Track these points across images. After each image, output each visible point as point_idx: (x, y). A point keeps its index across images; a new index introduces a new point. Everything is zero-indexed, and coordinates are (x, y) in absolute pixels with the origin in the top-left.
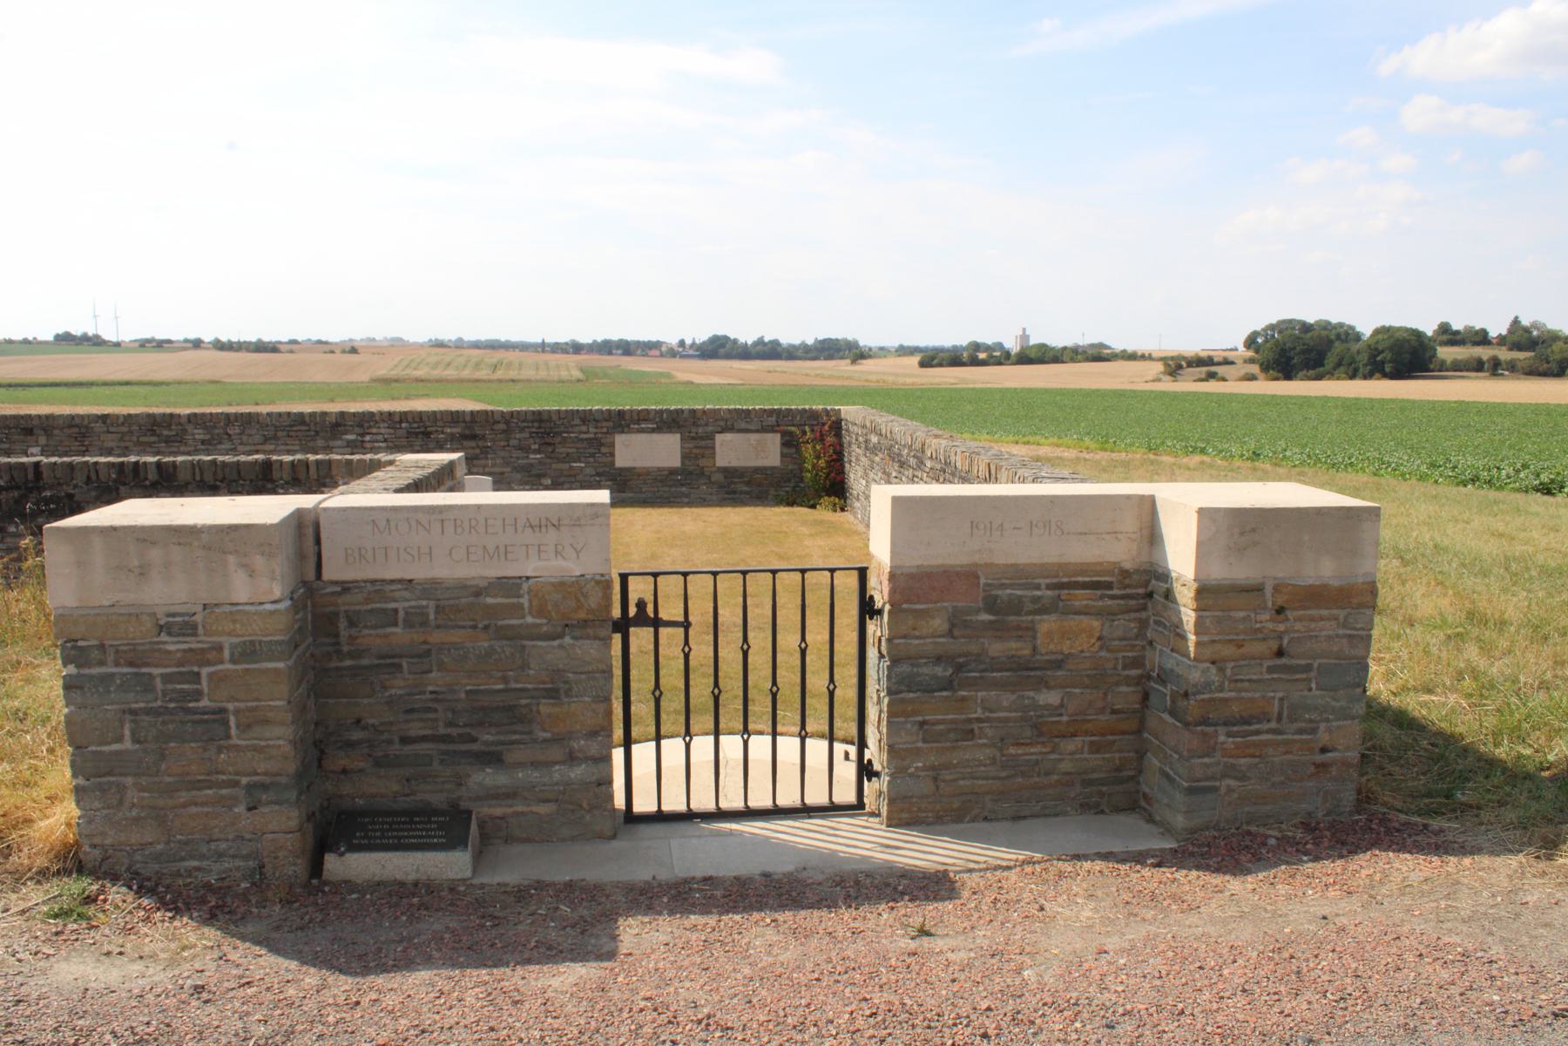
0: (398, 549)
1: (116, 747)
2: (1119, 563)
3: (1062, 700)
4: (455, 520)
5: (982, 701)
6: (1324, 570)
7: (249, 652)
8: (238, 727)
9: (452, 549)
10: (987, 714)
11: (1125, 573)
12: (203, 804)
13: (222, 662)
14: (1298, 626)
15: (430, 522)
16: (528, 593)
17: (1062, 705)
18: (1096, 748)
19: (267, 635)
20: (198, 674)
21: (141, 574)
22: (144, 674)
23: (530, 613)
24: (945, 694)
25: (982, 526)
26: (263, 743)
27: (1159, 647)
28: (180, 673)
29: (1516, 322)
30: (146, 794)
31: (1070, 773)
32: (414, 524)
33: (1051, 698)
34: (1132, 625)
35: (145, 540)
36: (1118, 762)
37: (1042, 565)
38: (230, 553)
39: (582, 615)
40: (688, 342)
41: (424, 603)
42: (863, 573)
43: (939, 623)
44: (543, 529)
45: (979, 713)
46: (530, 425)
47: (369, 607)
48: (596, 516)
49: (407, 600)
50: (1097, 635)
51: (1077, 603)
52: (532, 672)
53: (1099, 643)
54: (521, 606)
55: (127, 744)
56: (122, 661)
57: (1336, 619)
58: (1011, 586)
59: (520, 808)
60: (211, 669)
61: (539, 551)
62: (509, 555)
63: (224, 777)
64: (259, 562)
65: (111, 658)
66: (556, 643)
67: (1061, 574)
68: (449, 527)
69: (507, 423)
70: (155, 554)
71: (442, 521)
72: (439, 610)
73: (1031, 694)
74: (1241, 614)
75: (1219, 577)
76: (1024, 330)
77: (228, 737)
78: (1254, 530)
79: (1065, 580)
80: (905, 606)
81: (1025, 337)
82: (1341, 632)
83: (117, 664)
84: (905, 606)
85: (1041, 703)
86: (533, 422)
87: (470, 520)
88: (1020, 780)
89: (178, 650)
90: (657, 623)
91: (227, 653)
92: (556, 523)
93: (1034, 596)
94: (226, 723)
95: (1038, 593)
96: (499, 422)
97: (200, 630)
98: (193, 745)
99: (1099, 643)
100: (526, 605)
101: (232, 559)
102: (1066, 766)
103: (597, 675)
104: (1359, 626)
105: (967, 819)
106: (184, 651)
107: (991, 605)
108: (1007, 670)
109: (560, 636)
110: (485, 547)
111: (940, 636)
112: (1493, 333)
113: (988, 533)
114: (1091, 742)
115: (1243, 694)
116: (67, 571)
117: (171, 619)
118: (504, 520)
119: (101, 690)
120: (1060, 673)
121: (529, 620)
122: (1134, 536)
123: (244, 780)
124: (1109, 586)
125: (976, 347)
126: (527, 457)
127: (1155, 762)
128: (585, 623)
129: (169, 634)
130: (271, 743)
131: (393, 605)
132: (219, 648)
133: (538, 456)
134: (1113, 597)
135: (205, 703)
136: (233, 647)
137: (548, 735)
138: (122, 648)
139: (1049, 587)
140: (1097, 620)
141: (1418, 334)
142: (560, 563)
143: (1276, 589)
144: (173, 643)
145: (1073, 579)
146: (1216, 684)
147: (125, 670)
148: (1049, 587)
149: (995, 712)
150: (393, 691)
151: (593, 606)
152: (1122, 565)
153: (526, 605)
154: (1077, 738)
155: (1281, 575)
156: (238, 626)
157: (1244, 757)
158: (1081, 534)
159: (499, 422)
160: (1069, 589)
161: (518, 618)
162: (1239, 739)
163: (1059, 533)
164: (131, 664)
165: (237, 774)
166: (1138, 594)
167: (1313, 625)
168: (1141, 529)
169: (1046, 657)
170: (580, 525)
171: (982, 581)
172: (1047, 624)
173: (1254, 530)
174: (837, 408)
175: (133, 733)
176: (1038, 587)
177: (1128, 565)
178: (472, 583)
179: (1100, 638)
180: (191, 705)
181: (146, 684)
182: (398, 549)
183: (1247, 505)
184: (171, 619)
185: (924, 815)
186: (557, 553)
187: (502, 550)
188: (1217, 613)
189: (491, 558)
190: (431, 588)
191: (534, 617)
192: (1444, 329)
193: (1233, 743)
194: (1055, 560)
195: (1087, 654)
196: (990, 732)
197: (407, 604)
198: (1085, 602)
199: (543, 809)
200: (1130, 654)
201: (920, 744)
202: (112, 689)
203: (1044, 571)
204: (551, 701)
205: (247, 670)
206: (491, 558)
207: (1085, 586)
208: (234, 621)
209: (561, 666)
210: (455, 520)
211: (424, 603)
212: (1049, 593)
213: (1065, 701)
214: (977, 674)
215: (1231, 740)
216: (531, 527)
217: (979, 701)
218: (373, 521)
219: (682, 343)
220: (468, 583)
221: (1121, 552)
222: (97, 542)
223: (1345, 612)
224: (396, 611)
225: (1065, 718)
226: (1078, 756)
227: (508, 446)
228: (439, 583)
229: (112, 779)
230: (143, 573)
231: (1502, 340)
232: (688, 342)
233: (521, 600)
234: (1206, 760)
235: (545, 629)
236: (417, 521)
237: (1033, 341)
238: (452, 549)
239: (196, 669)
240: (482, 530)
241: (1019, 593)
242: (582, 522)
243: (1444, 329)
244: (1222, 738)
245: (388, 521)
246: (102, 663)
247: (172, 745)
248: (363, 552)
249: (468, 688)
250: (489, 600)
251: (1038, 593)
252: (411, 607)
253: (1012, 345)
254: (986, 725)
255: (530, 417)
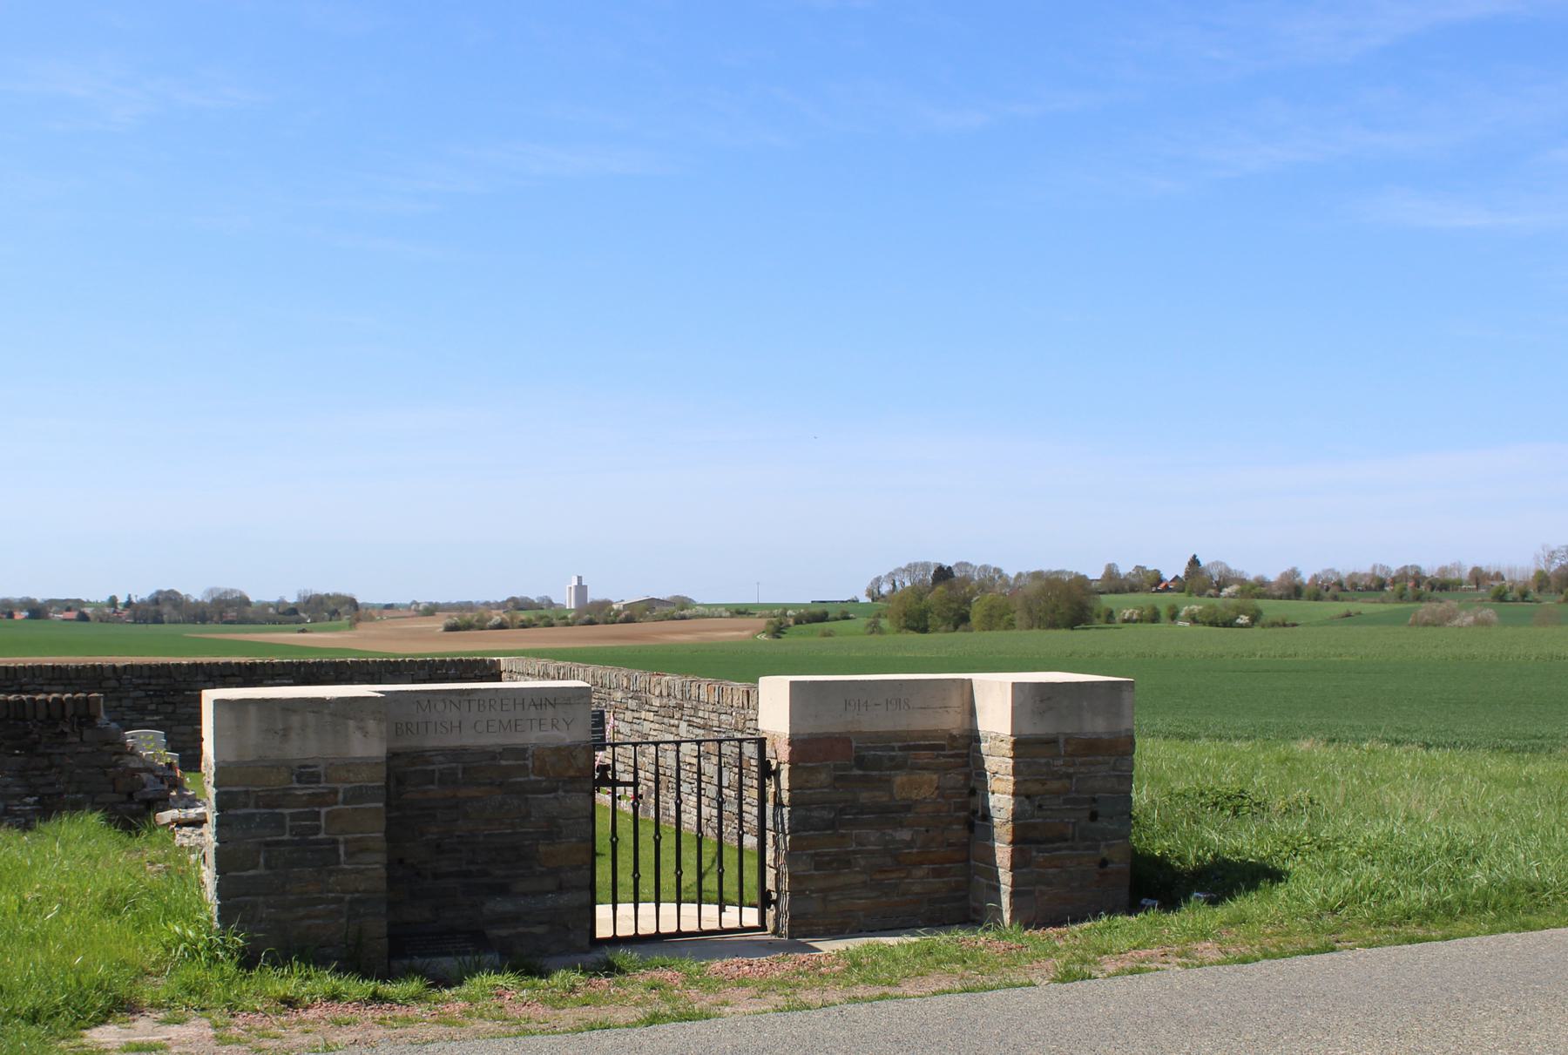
0: (436, 723)
1: (251, 872)
2: (949, 730)
3: (912, 835)
4: (479, 700)
5: (856, 837)
6: (1096, 725)
7: (357, 795)
8: (346, 854)
9: (476, 723)
10: (859, 848)
11: (953, 738)
12: (316, 917)
13: (336, 804)
14: (1083, 769)
15: (460, 702)
16: (532, 756)
17: (913, 840)
18: (937, 873)
19: (373, 782)
20: (319, 813)
21: (285, 735)
22: (277, 814)
23: (533, 772)
24: (829, 832)
25: (853, 703)
26: (363, 867)
27: (981, 792)
28: (301, 813)
29: (1194, 562)
30: (273, 910)
31: (921, 894)
32: (448, 703)
33: (905, 835)
34: (960, 777)
35: (288, 710)
36: (953, 884)
37: (895, 732)
38: (351, 719)
39: (572, 773)
40: (122, 599)
41: (454, 765)
42: (761, 743)
43: (823, 777)
44: (544, 707)
45: (854, 847)
46: (147, 681)
47: (413, 769)
48: (582, 697)
49: (442, 763)
50: (936, 785)
51: (920, 761)
52: (533, 819)
53: (937, 792)
54: (526, 766)
55: (261, 871)
56: (261, 804)
57: (1108, 763)
58: (874, 749)
59: (521, 930)
60: (329, 809)
61: (540, 725)
62: (518, 727)
63: (333, 895)
64: (371, 725)
65: (252, 802)
66: (552, 795)
67: (908, 739)
68: (474, 706)
69: (119, 680)
70: (295, 720)
71: (469, 701)
72: (465, 770)
73: (890, 831)
74: (1043, 761)
75: (1027, 733)
76: (580, 578)
77: (338, 863)
78: (1049, 699)
79: (912, 743)
80: (800, 764)
81: (581, 590)
82: (1112, 773)
83: (257, 807)
84: (800, 764)
85: (897, 838)
86: (150, 677)
87: (490, 700)
88: (884, 899)
89: (304, 795)
90: (615, 783)
91: (340, 797)
92: (552, 702)
93: (890, 756)
94: (336, 851)
95: (894, 753)
96: (109, 679)
97: (323, 779)
98: (311, 869)
99: (937, 792)
100: (531, 766)
101: (351, 723)
102: (917, 888)
103: (581, 820)
104: (1124, 768)
105: (847, 931)
106: (309, 795)
107: (860, 762)
108: (873, 813)
109: (555, 790)
110: (500, 722)
111: (825, 787)
112: (1168, 576)
113: (857, 708)
114: (933, 869)
115: (1048, 820)
116: (229, 733)
117: (302, 770)
118: (515, 700)
119: (244, 826)
120: (909, 815)
121: (532, 777)
122: (958, 710)
123: (348, 897)
124: (942, 747)
125: (518, 604)
126: (143, 719)
127: (982, 880)
128: (573, 780)
129: (299, 781)
130: (370, 867)
131: (431, 767)
132: (335, 792)
133: (156, 718)
134: (945, 756)
135: (322, 836)
136: (346, 791)
137: (543, 869)
138: (260, 794)
139: (901, 749)
140: (935, 774)
141: (1082, 581)
142: (556, 732)
143: (1067, 741)
144: (302, 789)
145: (918, 743)
146: (1030, 812)
147: (263, 811)
148: (901, 749)
149: (865, 846)
150: (429, 836)
151: (581, 766)
152: (952, 731)
153: (531, 766)
154: (924, 866)
155: (1069, 731)
156: (351, 775)
157: (1051, 868)
158: (922, 708)
159: (109, 679)
160: (914, 750)
161: (524, 777)
162: (1046, 854)
163: (906, 707)
164: (266, 806)
165: (343, 892)
166: (963, 754)
167: (1092, 769)
168: (963, 705)
169: (900, 803)
170: (570, 704)
171: (854, 744)
172: (900, 778)
173: (1049, 699)
174: (495, 659)
175: (266, 861)
176: (893, 749)
177: (955, 732)
178: (491, 749)
179: (937, 788)
180: (311, 838)
181: (279, 822)
182: (436, 723)
183: (1044, 681)
184: (302, 770)
185: (816, 928)
186: (553, 725)
187: (513, 723)
188: (1028, 760)
189: (505, 729)
190: (457, 753)
191: (535, 775)
192: (1111, 573)
193: (1043, 856)
194: (905, 728)
195: (929, 801)
196: (862, 863)
197: (442, 766)
198: (926, 760)
199: (539, 930)
200: (959, 800)
201: (813, 872)
202: (253, 826)
203: (895, 735)
204: (547, 842)
205: (356, 809)
206: (505, 729)
207: (926, 748)
208: (349, 771)
209: (555, 814)
210: (479, 700)
211: (454, 765)
212: (900, 753)
213: (915, 837)
214: (850, 817)
215: (1041, 854)
216: (534, 705)
217: (854, 837)
218: (418, 701)
219: (113, 601)
220: (487, 749)
221: (951, 722)
222: (252, 709)
223: (1113, 759)
224: (433, 771)
225: (915, 850)
226: (926, 880)
227: (121, 706)
228: (466, 750)
229: (247, 898)
230: (285, 734)
231: (1180, 585)
232: (122, 599)
233: (526, 762)
234: (1024, 870)
235: (544, 784)
236: (451, 701)
237: (594, 595)
238: (476, 723)
239: (317, 809)
240: (499, 708)
241: (880, 753)
242: (572, 702)
243: (1111, 573)
244: (1034, 854)
245: (429, 701)
246: (246, 806)
247: (295, 870)
248: (409, 726)
249: (486, 832)
250: (503, 763)
251: (894, 753)
252: (444, 769)
253: (568, 601)
254: (859, 856)
255: (146, 673)
